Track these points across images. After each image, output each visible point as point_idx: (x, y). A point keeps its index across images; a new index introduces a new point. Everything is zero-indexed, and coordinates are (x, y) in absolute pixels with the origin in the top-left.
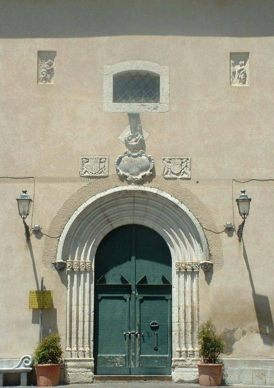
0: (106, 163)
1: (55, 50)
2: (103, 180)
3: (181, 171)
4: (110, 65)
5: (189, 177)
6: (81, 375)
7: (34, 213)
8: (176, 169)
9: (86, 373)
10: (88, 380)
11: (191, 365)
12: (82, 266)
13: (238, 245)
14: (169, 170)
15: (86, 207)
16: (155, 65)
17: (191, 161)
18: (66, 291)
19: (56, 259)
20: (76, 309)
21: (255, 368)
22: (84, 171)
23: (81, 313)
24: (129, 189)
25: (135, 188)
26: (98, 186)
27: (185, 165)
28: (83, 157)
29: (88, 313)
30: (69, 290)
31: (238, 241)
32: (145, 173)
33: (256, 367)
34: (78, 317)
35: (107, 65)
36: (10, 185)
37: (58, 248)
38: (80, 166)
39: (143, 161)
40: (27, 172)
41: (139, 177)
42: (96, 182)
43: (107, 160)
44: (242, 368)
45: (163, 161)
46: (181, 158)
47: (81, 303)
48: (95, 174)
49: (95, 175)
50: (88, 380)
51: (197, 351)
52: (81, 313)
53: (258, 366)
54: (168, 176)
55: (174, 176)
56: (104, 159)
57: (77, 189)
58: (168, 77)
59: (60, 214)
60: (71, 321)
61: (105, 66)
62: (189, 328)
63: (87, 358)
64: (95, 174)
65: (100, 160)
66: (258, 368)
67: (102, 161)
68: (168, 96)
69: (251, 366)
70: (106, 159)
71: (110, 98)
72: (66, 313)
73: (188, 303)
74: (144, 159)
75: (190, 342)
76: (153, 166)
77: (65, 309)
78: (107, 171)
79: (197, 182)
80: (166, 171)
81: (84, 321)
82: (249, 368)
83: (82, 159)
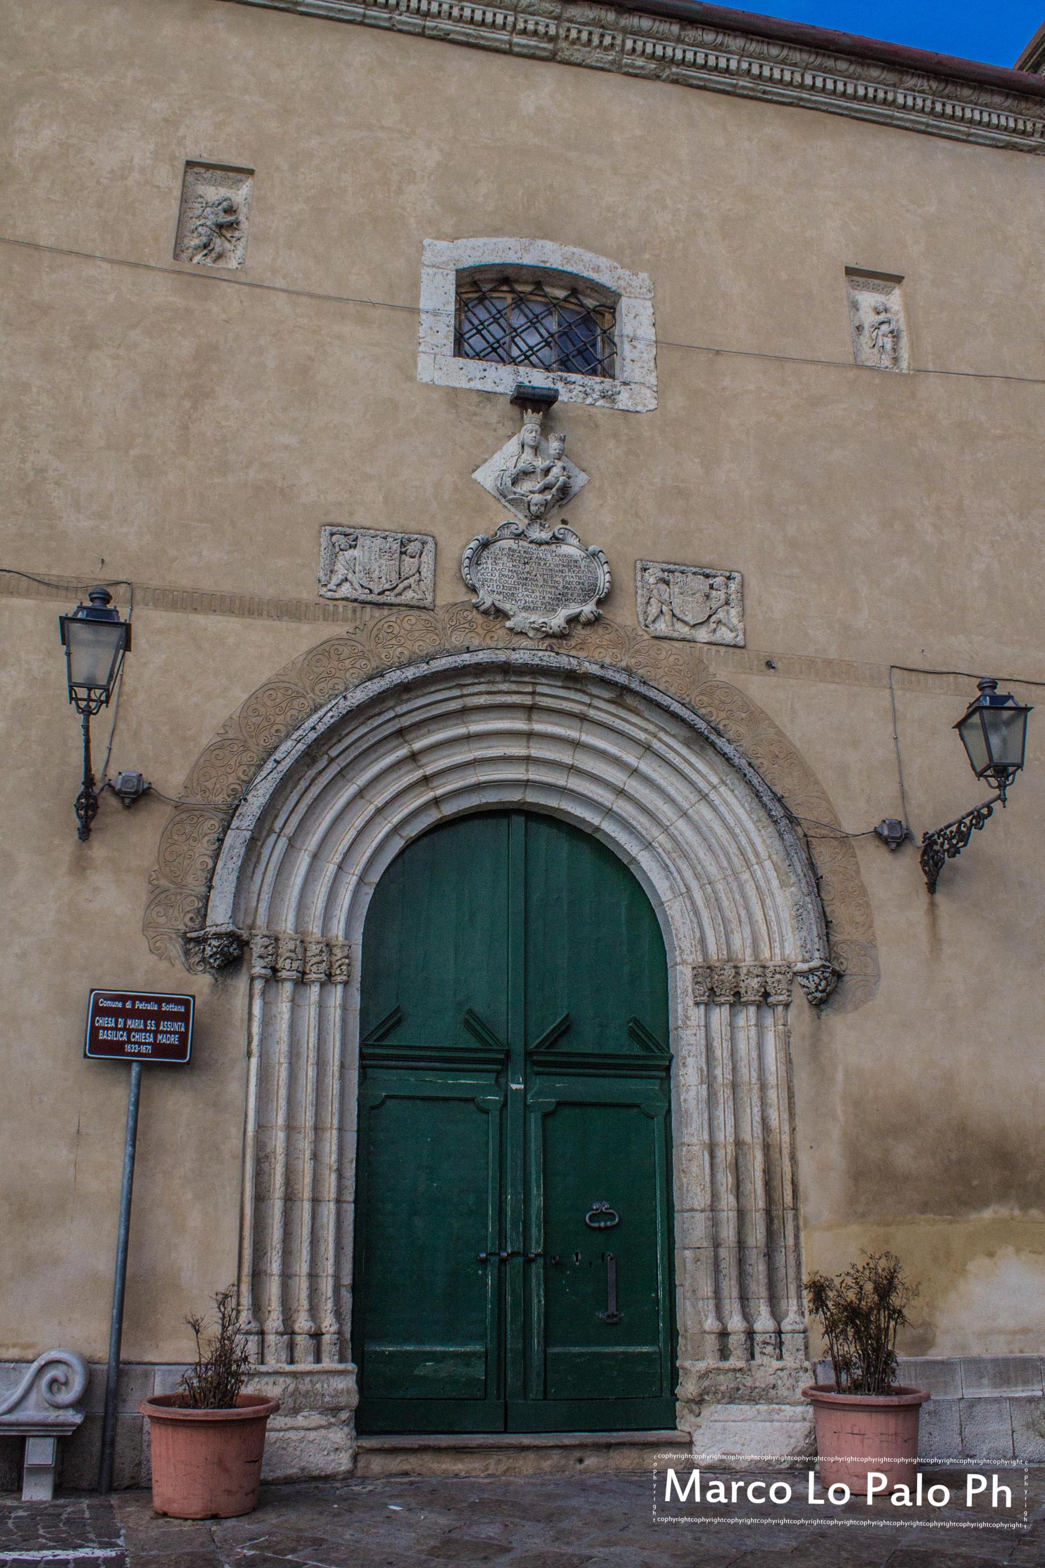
0: (427, 558)
1: (251, 166)
2: (414, 621)
3: (710, 616)
4: (444, 240)
5: (740, 641)
6: (301, 1441)
7: (121, 726)
8: (264, 705)
9: (323, 1431)
10: (333, 1465)
11: (772, 1392)
12: (312, 962)
13: (925, 906)
14: (664, 608)
15: (344, 712)
16: (603, 262)
17: (742, 586)
18: (244, 1064)
19: (205, 920)
20: (284, 1145)
21: (1016, 1391)
22: (335, 580)
23: (306, 1167)
24: (521, 661)
25: (541, 660)
26: (394, 642)
27: (723, 597)
28: (335, 529)
29: (335, 1167)
30: (254, 1061)
31: (923, 889)
32: (578, 610)
33: (1020, 1388)
34: (288, 1182)
35: (437, 238)
36: (30, 603)
37: (216, 877)
38: (323, 561)
39: (572, 564)
40: (103, 561)
41: (557, 620)
42: (386, 626)
43: (430, 546)
44: (970, 1393)
45: (642, 576)
46: (708, 571)
47: (306, 1118)
48: (379, 594)
49: (382, 599)
50: (333, 1465)
51: (793, 1332)
52: (306, 1167)
53: (1026, 1382)
54: (662, 627)
55: (684, 631)
56: (418, 544)
57: (305, 647)
58: (649, 304)
59: (231, 736)
60: (260, 1198)
61: (427, 241)
62: (757, 1236)
63: (327, 1364)
64: (379, 594)
65: (402, 544)
66: (1029, 1394)
67: (412, 548)
68: (652, 364)
69: (1001, 1385)
70: (424, 543)
71: (445, 341)
72: (239, 1162)
73: (752, 1133)
74: (575, 558)
75: (763, 1292)
76: (607, 585)
77: (236, 1142)
78: (430, 585)
79: (769, 665)
80: (653, 610)
81: (315, 1201)
82: (996, 1394)
83: (332, 534)
